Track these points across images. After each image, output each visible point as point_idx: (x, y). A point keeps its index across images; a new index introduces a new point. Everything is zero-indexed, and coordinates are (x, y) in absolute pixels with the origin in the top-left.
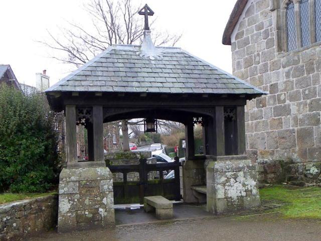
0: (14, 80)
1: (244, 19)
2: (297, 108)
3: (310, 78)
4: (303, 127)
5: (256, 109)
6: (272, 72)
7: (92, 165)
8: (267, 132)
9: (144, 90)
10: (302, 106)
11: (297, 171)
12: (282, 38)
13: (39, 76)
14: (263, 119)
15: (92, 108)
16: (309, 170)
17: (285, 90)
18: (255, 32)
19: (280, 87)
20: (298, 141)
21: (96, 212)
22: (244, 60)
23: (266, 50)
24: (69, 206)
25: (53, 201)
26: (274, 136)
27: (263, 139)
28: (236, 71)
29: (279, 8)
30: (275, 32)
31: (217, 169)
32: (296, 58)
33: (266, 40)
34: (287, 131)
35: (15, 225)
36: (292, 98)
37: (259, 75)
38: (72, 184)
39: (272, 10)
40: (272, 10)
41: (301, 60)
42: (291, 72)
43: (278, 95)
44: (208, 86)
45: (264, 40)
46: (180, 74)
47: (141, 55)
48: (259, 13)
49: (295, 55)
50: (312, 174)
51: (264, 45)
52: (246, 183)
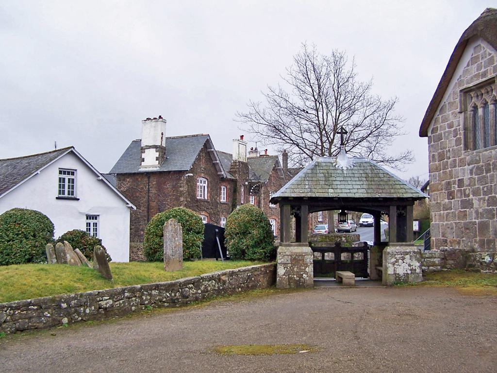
0: (213, 150)
1: (439, 116)
2: (478, 202)
3: (487, 177)
4: (482, 220)
5: (447, 201)
7: (300, 245)
8: (455, 223)
11: (475, 259)
12: (469, 138)
13: (237, 143)
14: (453, 210)
15: (301, 207)
16: (484, 259)
17: (469, 185)
18: (447, 130)
19: (466, 182)
20: (479, 232)
22: (438, 154)
23: (455, 147)
24: (284, 271)
25: (273, 268)
26: (460, 227)
27: (452, 229)
28: (431, 163)
29: (467, 110)
30: (462, 132)
33: (455, 138)
34: (470, 222)
35: (253, 279)
36: (475, 193)
37: (450, 169)
38: (286, 257)
39: (461, 112)
40: (461, 112)
41: (481, 160)
42: (474, 171)
44: (384, 191)
46: (364, 182)
47: (336, 166)
48: (450, 112)
50: (485, 262)
51: (454, 143)
52: (411, 264)
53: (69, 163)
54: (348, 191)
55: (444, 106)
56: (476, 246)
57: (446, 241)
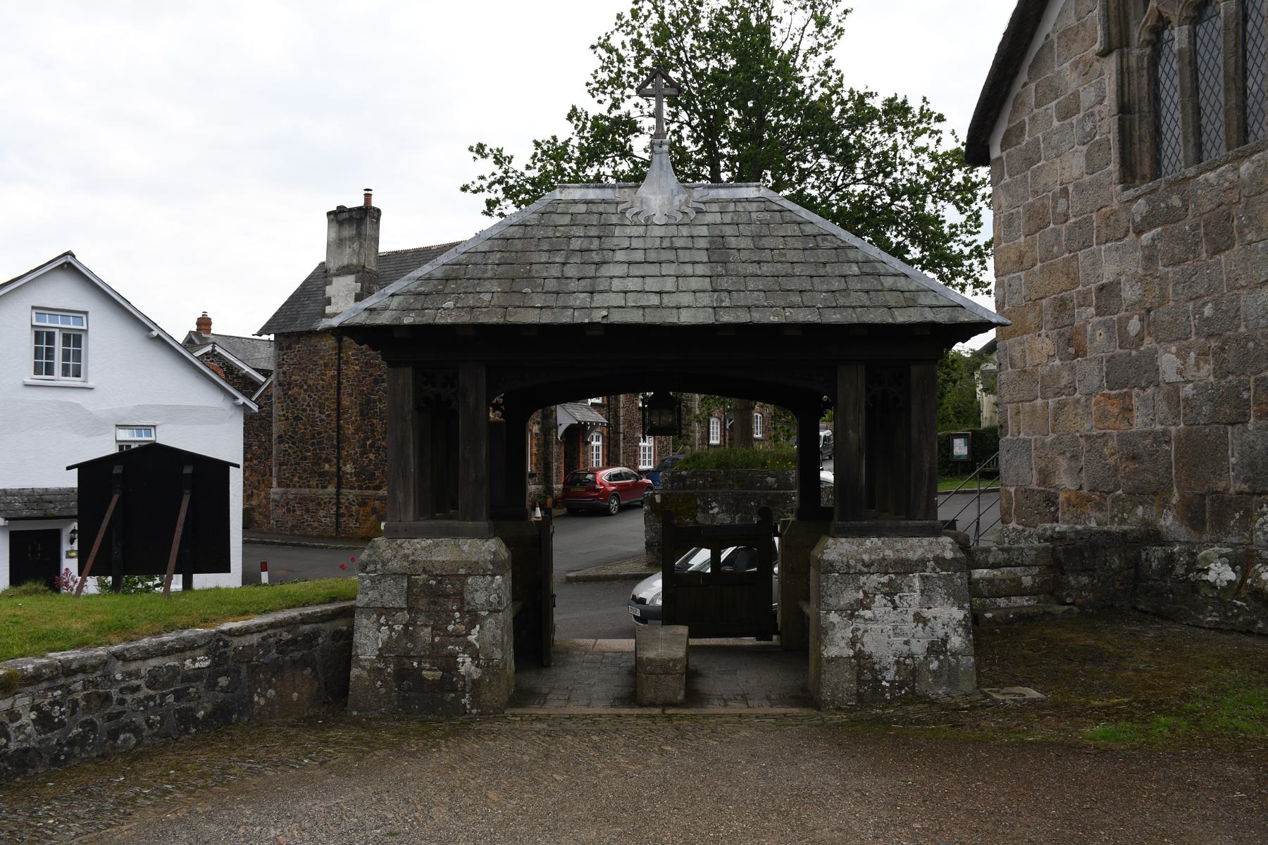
1: (1026, 87)
2: (1179, 362)
6: (1103, 247)
9: (597, 316)
10: (1192, 355)
12: (1136, 140)
21: (450, 665)
23: (1087, 178)
29: (1128, 45)
31: (831, 564)
32: (1176, 201)
33: (1085, 148)
34: (1145, 435)
37: (1067, 255)
39: (1104, 54)
40: (1104, 54)
43: (1119, 319)
45: (1082, 147)
48: (1067, 65)
49: (1172, 192)
50: (1213, 586)
52: (927, 613)
53: (63, 294)
54: (654, 300)
55: (1046, 50)
56: (1168, 522)
57: (1051, 500)
